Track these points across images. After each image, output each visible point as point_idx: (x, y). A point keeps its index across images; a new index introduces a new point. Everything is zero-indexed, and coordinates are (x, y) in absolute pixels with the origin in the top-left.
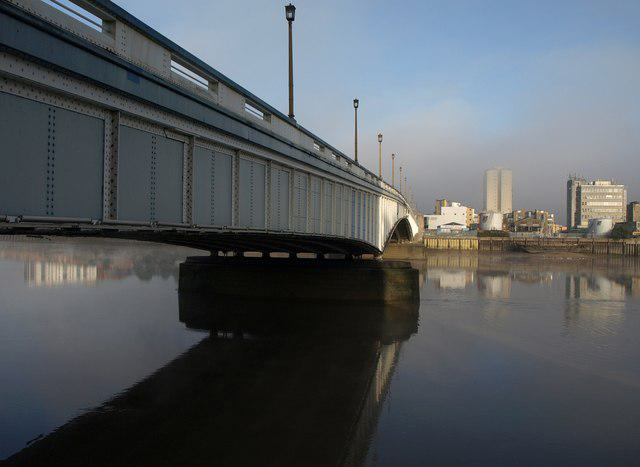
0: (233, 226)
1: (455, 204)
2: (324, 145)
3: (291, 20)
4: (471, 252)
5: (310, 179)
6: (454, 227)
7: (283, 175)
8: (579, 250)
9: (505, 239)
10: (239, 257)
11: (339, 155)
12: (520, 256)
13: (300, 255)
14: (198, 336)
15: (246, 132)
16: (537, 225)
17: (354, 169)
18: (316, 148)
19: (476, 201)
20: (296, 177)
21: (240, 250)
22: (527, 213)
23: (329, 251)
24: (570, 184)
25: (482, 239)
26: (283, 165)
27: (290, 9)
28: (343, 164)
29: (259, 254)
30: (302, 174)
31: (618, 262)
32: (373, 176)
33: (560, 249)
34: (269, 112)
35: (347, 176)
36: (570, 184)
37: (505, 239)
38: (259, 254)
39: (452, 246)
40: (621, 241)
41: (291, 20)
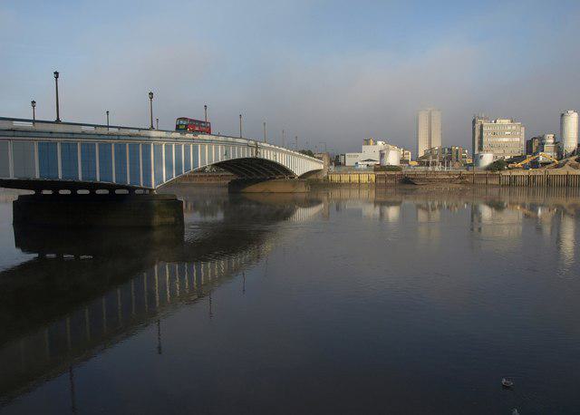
1: (380, 143)
3: (57, 78)
4: (370, 185)
6: (370, 163)
8: (459, 181)
9: (398, 173)
10: (56, 194)
12: (409, 187)
14: (20, 257)
19: (405, 141)
22: (444, 149)
24: (474, 122)
25: (380, 173)
31: (495, 192)
33: (443, 180)
36: (474, 122)
37: (398, 173)
39: (353, 180)
40: (498, 172)
41: (57, 78)
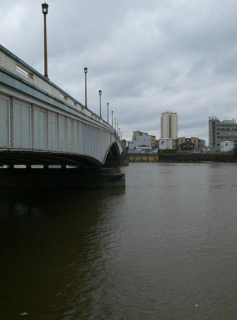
0: (10, 146)
2: (67, 96)
3: (45, 13)
5: (58, 117)
7: (42, 114)
11: (76, 103)
13: (33, 167)
15: (18, 85)
16: (192, 146)
17: (85, 111)
18: (61, 97)
20: (49, 115)
21: (11, 165)
23: (70, 164)
26: (41, 108)
27: (45, 6)
28: (78, 108)
29: (24, 167)
30: (53, 114)
32: (97, 116)
34: (33, 73)
35: (81, 116)
38: (24, 167)
41: (45, 13)
